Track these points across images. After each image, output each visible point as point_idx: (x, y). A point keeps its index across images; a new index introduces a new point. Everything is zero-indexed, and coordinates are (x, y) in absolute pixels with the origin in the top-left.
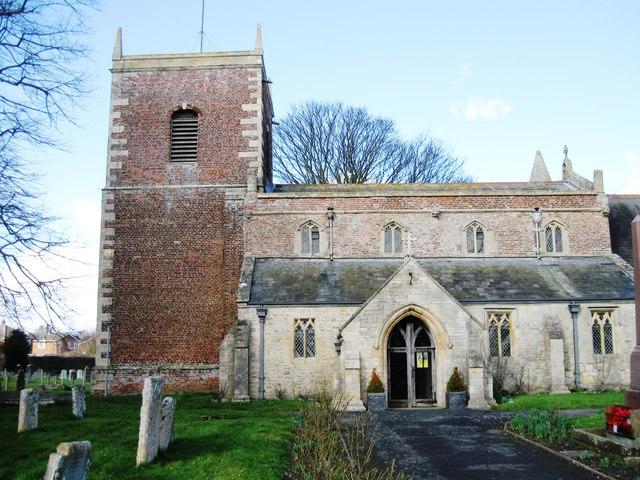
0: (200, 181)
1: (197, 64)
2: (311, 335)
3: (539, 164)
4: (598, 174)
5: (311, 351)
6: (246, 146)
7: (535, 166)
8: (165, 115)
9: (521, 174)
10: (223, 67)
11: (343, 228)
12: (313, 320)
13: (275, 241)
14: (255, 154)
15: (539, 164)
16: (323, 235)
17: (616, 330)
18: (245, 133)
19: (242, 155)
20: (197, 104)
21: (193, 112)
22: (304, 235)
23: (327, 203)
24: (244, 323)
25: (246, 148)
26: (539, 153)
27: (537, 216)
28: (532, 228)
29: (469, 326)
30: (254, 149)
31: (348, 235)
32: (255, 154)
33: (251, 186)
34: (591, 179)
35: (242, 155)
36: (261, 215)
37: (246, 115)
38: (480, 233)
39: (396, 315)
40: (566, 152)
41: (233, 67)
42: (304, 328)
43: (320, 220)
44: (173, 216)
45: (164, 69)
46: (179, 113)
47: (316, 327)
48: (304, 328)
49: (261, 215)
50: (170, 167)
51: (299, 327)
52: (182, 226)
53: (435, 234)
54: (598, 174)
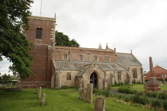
0: (42, 43)
1: (42, 19)
2: (70, 76)
3: (100, 46)
4: (115, 49)
5: (70, 79)
6: (52, 37)
7: (100, 46)
8: (35, 29)
9: (97, 47)
10: (48, 21)
11: (72, 55)
12: (70, 73)
13: (58, 57)
14: (54, 39)
15: (100, 46)
16: (68, 56)
17: (122, 76)
18: (52, 34)
19: (51, 39)
20: (42, 27)
21: (41, 29)
22: (64, 56)
23: (69, 50)
24: (57, 73)
25: (52, 37)
26: (100, 44)
27: (106, 55)
28: (104, 57)
29: (104, 74)
30: (54, 38)
31: (73, 56)
32: (54, 39)
33: (54, 45)
34: (114, 50)
35: (51, 39)
36: (55, 51)
37: (52, 31)
38: (96, 58)
39: (92, 72)
40: (107, 44)
41: (50, 21)
42: (69, 74)
43: (67, 53)
44: (36, 50)
45: (35, 19)
46: (38, 29)
47: (71, 74)
48: (69, 74)
49: (55, 51)
50: (36, 40)
51: (68, 74)
52: (38, 52)
53: (88, 58)
54: (115, 49)
